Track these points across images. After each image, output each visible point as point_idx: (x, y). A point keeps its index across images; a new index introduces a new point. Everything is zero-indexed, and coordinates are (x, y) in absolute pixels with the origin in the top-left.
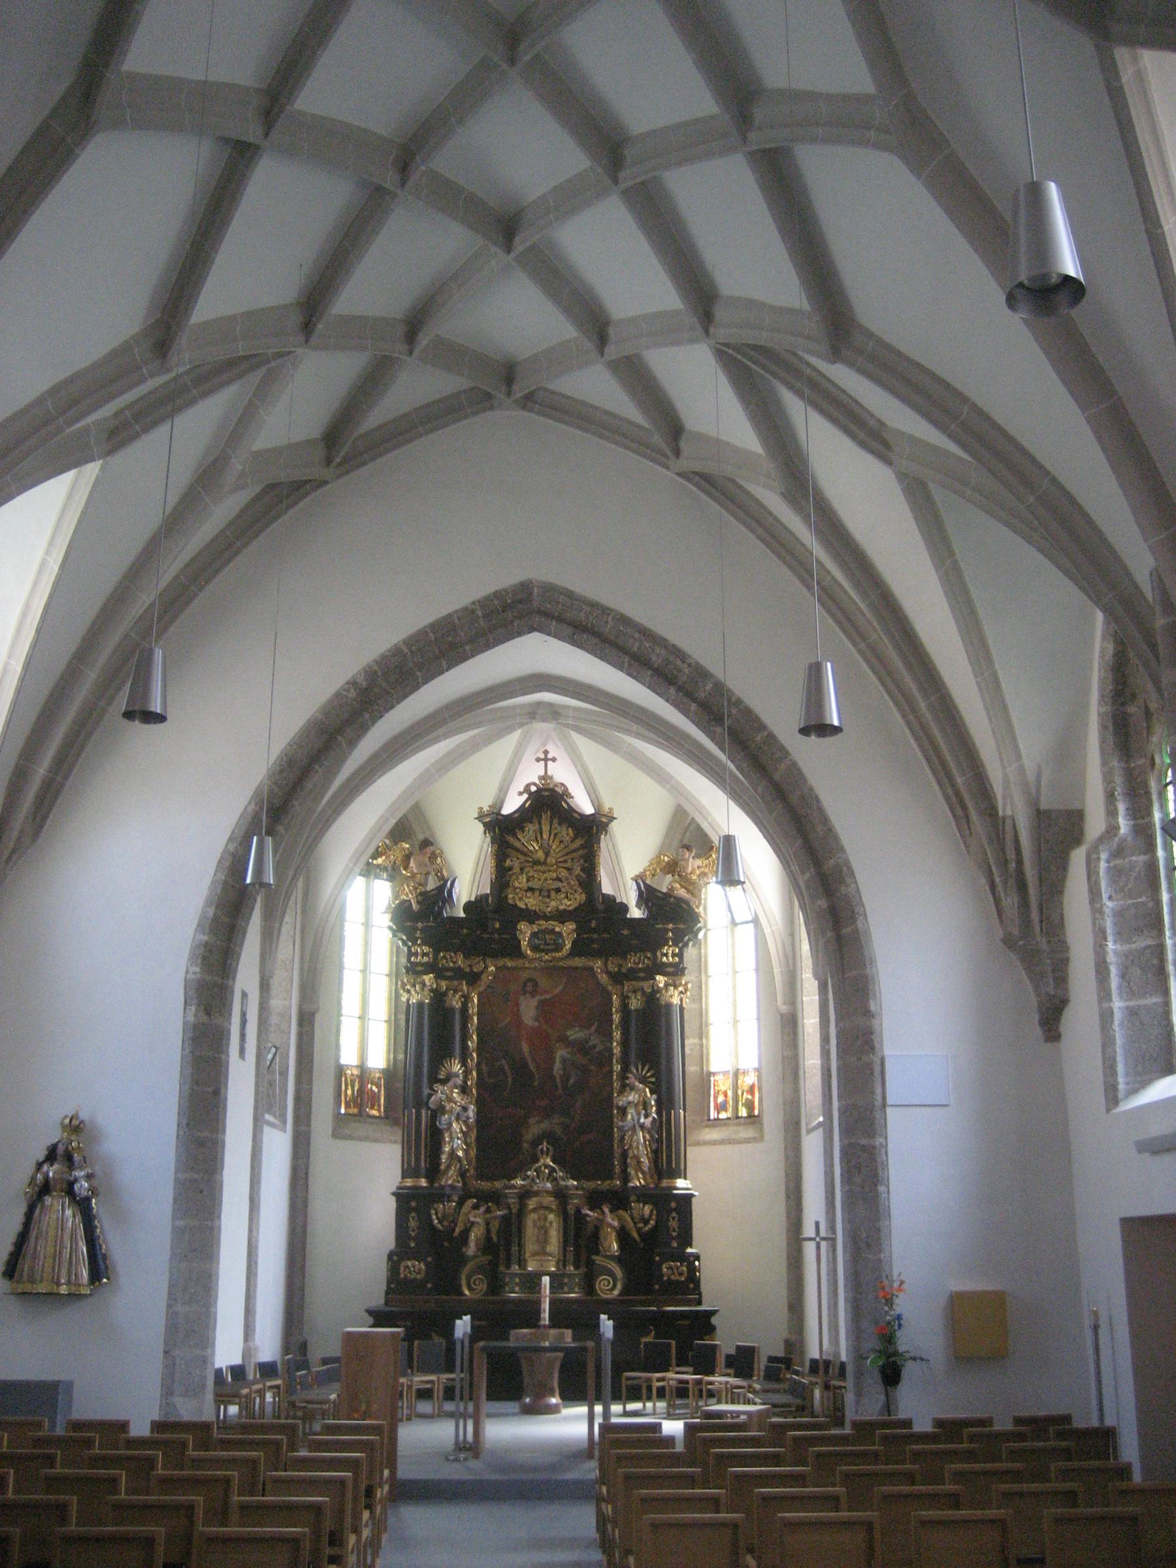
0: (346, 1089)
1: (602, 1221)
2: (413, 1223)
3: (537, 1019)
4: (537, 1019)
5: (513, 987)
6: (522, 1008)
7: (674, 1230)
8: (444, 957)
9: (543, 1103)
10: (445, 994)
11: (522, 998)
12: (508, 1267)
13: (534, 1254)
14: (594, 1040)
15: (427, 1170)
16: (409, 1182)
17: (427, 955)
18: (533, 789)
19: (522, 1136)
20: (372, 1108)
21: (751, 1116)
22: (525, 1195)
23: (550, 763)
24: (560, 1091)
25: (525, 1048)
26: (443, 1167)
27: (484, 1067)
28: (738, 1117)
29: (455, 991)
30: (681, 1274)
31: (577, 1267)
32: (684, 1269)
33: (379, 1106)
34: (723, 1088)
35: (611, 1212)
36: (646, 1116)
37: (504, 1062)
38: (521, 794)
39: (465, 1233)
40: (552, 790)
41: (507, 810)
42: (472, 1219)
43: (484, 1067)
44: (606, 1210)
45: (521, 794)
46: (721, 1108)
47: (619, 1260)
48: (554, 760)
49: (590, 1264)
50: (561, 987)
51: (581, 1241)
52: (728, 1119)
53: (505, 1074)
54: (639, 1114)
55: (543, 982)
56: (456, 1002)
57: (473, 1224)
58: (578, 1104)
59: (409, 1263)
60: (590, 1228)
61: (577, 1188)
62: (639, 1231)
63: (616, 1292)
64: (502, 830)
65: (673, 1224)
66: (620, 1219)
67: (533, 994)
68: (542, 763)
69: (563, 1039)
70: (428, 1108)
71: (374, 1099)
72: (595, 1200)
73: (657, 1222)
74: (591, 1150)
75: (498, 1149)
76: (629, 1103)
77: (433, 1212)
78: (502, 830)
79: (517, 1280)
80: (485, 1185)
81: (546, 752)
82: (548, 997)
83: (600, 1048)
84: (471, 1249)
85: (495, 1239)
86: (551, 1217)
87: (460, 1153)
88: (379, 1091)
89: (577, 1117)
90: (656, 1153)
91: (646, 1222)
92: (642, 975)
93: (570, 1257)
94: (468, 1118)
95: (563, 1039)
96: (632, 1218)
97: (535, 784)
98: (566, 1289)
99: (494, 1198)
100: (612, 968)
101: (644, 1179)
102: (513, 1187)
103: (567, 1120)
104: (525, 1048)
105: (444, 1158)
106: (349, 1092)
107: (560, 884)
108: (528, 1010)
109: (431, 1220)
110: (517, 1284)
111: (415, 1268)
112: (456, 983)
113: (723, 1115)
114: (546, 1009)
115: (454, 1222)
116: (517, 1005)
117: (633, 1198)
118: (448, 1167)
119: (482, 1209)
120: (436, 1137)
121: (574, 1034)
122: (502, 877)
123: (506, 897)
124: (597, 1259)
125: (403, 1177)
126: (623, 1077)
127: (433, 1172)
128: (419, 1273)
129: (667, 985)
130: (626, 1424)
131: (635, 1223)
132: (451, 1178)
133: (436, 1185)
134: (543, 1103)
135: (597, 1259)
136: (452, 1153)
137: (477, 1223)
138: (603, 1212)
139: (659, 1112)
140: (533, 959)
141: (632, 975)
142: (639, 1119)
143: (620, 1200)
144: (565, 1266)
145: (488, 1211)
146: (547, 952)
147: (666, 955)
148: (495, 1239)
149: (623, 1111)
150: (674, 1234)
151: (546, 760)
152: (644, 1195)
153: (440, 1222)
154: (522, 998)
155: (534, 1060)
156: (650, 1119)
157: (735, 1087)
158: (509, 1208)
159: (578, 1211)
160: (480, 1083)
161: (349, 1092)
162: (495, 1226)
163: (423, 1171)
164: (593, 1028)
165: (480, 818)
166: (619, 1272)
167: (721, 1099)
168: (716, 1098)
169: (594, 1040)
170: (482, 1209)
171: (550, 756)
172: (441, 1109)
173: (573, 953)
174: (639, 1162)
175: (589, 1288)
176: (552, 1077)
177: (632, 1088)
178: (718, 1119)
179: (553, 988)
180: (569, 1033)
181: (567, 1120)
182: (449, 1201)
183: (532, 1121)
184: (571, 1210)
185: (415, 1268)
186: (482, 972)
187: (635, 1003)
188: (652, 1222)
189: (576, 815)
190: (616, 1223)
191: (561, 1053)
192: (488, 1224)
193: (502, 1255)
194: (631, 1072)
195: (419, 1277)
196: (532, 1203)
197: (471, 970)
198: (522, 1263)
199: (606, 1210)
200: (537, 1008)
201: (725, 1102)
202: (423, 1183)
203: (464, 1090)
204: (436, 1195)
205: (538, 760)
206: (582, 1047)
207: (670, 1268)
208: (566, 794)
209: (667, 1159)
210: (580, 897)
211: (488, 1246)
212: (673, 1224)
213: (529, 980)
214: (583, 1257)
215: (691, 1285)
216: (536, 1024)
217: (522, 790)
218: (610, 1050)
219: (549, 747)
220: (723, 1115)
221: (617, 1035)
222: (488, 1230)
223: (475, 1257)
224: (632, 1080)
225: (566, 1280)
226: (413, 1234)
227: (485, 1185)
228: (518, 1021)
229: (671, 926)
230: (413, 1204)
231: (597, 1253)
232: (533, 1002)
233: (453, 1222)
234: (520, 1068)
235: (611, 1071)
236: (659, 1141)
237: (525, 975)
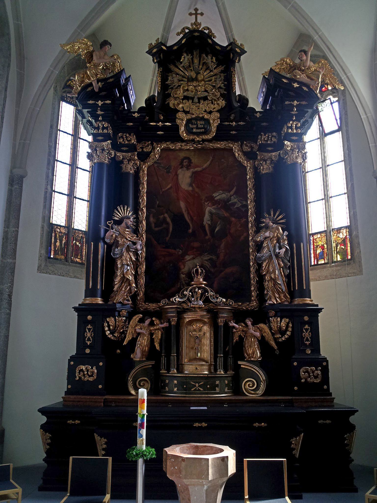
0: (56, 242)
1: (246, 332)
2: (88, 334)
3: (191, 185)
4: (191, 185)
5: (174, 164)
6: (180, 177)
7: (307, 340)
8: (122, 137)
9: (196, 244)
10: (122, 162)
11: (180, 171)
12: (168, 370)
13: (190, 360)
14: (234, 200)
15: (102, 291)
16: (89, 301)
17: (107, 128)
18: (187, 31)
19: (180, 269)
20: (76, 256)
21: (344, 260)
22: (181, 312)
23: (199, 16)
24: (209, 236)
25: (182, 205)
26: (115, 289)
27: (152, 219)
28: (333, 262)
29: (129, 161)
30: (316, 377)
31: (226, 371)
32: (319, 372)
33: (82, 256)
34: (320, 243)
35: (253, 324)
36: (280, 248)
37: (166, 215)
38: (178, 34)
39: (133, 342)
40: (202, 32)
41: (170, 43)
42: (138, 331)
43: (152, 219)
44: (249, 323)
45: (178, 34)
46: (321, 256)
47: (262, 364)
48: (202, 14)
49: (237, 368)
50: (208, 163)
51: (228, 349)
52: (325, 264)
53: (168, 224)
54: (275, 247)
55: (195, 160)
56: (130, 168)
57: (139, 334)
58: (222, 246)
59: (83, 368)
60: (236, 339)
61: (225, 304)
62: (276, 340)
63: (260, 392)
64: (165, 57)
65: (307, 335)
66: (261, 331)
67: (188, 167)
68: (194, 16)
69: (211, 199)
70: (105, 243)
71: (77, 251)
72: (239, 316)
73: (292, 332)
74: (235, 279)
75: (162, 279)
76: (266, 238)
77: (106, 324)
78: (165, 57)
79: (176, 382)
80: (152, 306)
81: (196, 10)
82: (199, 169)
83: (239, 205)
84: (137, 355)
85: (158, 347)
86: (206, 328)
87: (130, 278)
88: (82, 246)
89: (222, 256)
90: (289, 278)
91: (283, 333)
92: (270, 149)
93: (220, 361)
94: (137, 250)
95: (211, 199)
96: (271, 329)
97: (188, 28)
98: (218, 389)
99: (160, 314)
100: (246, 149)
101: (280, 298)
102: (173, 303)
103: (214, 257)
104: (182, 205)
105: (117, 280)
106: (58, 244)
107: (206, 94)
108: (185, 178)
109: (104, 331)
110: (176, 386)
111: (89, 372)
112: (130, 154)
113: (322, 262)
114: (196, 177)
115: (124, 333)
116: (177, 175)
117: (272, 313)
118: (120, 287)
119: (147, 322)
120: (110, 264)
121: (219, 195)
122: (165, 88)
123: (169, 103)
124: (243, 364)
125: (86, 297)
126: (258, 221)
127: (108, 292)
128: (92, 376)
129: (292, 150)
130: (101, 222)
131: (273, 334)
132: (121, 297)
133: (110, 303)
134: (196, 244)
135: (243, 364)
136: (124, 279)
137: (142, 335)
138: (247, 326)
139: (290, 244)
140: (187, 142)
141: (263, 148)
142: (274, 250)
143: (260, 316)
144: (216, 370)
145: (152, 324)
146: (198, 134)
147: (291, 128)
148: (158, 347)
149: (259, 247)
150: (308, 343)
151: (196, 14)
152: (281, 311)
153: (112, 333)
154: (180, 171)
155: (188, 213)
156: (284, 250)
157: (329, 242)
158: (169, 321)
159: (226, 324)
160: (149, 230)
161: (58, 244)
162: (158, 335)
163: (99, 292)
164: (232, 193)
165: (149, 52)
166: (262, 376)
167: (319, 251)
168: (315, 251)
169: (234, 200)
170: (147, 322)
171: (199, 12)
172: (116, 244)
173: (216, 139)
174: (275, 284)
175: (236, 389)
176: (203, 227)
177: (267, 227)
178: (318, 264)
179: (202, 164)
180: (214, 195)
181: (214, 257)
182: (119, 316)
183: (188, 258)
184: (221, 322)
185: (89, 372)
186: (151, 152)
187: (265, 168)
188: (288, 333)
189: (218, 48)
190: (258, 334)
191: (209, 209)
192: (151, 334)
193: (163, 360)
194: (265, 218)
195: (91, 379)
196: (188, 317)
197: (143, 151)
198: (180, 369)
199: (249, 323)
200: (191, 177)
201: (323, 252)
202: (99, 301)
203: (136, 231)
204: (109, 310)
205: (191, 14)
206: (225, 205)
207: (307, 371)
208: (210, 36)
209: (296, 285)
210: (222, 103)
211: (152, 353)
212: (307, 335)
213: (185, 158)
214: (230, 361)
215: (322, 388)
216: (191, 189)
217: (180, 31)
218: (246, 206)
219: (198, 6)
220: (322, 262)
221: (251, 195)
222: (152, 341)
223: (140, 362)
224: (267, 221)
225: (217, 382)
226: (89, 343)
227: (152, 306)
228: (177, 186)
229: (295, 103)
230: (89, 317)
231: (243, 359)
232: (188, 174)
233: (123, 332)
234: (178, 219)
235: (247, 222)
236: (291, 268)
237: (182, 155)
